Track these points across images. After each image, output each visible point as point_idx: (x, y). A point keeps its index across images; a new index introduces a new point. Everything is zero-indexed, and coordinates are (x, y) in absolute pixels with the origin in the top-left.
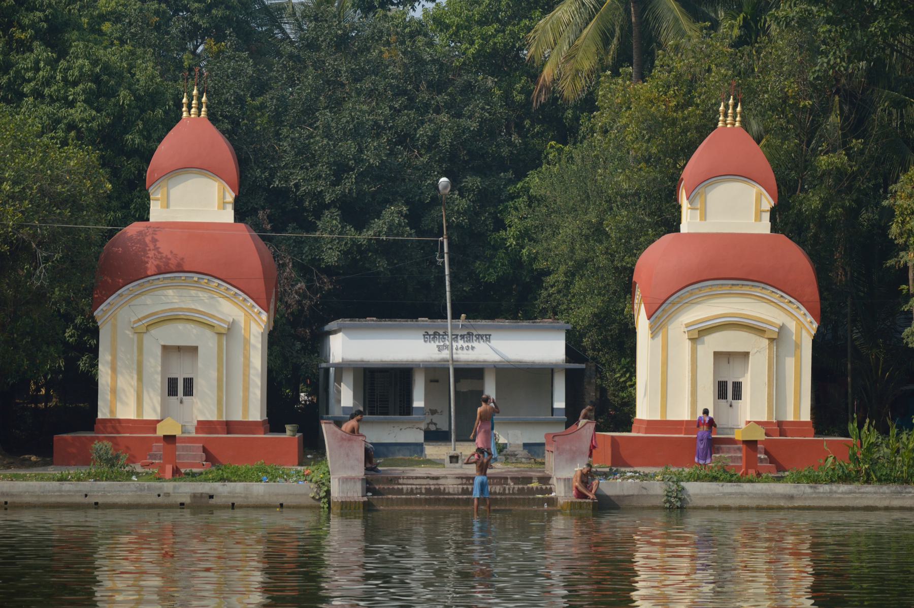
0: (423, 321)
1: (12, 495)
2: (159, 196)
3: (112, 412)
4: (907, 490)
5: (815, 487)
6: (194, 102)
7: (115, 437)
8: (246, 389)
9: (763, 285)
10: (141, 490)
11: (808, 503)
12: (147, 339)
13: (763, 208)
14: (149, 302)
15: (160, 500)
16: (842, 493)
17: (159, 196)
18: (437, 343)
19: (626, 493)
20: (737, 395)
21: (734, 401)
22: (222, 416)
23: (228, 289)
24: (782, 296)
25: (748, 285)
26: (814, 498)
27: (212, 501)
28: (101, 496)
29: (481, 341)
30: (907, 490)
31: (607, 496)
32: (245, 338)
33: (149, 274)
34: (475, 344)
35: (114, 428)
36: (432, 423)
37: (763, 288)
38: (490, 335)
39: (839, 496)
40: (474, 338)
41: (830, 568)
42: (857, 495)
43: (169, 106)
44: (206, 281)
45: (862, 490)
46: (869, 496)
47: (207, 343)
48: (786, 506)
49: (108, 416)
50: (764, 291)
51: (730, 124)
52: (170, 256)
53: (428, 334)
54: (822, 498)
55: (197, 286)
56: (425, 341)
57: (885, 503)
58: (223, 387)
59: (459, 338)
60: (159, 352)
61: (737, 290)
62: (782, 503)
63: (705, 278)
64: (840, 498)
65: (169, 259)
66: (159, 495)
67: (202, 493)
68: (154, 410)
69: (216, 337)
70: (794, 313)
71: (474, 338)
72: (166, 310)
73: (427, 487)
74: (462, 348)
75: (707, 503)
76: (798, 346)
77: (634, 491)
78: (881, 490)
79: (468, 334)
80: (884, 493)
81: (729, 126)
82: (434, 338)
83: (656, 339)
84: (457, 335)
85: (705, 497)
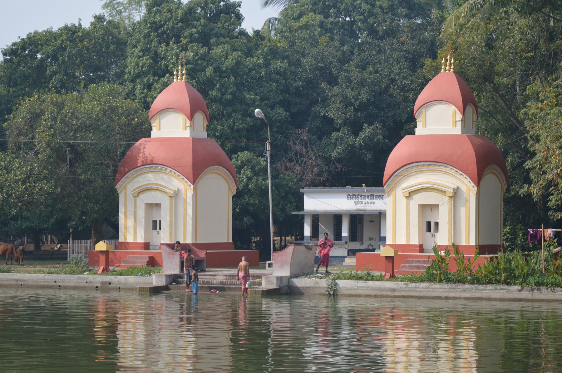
0: (349, 188)
1: (38, 281)
2: (155, 124)
3: (125, 238)
4: (458, 287)
5: (407, 284)
6: (179, 73)
7: (115, 252)
8: (185, 226)
9: (445, 165)
10: (79, 279)
11: (403, 294)
12: (138, 199)
13: (457, 119)
14: (141, 180)
15: (87, 285)
16: (422, 288)
17: (155, 124)
18: (355, 200)
19: (307, 286)
20: (436, 230)
21: (435, 233)
22: (172, 241)
23: (175, 173)
24: (456, 171)
25: (432, 165)
26: (406, 291)
27: (110, 286)
28: (62, 282)
29: (378, 199)
30: (458, 287)
31: (298, 287)
32: (184, 199)
33: (139, 165)
34: (375, 201)
35: (125, 246)
36: (370, 245)
37: (440, 165)
38: (383, 196)
39: (420, 290)
40: (375, 197)
41: (219, 332)
42: (430, 290)
43: (262, 75)
44: (160, 168)
45: (433, 287)
46: (437, 290)
47: (166, 203)
48: (391, 295)
49: (123, 241)
50: (446, 168)
51: (448, 70)
52: (148, 156)
53: (349, 195)
54: (410, 291)
55: (161, 171)
56: (348, 199)
57: (446, 295)
58: (174, 225)
59: (366, 197)
60: (143, 207)
61: (431, 168)
62: (389, 293)
63: (418, 161)
64: (420, 291)
65: (148, 157)
66: (87, 282)
67: (106, 282)
68: (142, 237)
69: (169, 198)
70: (464, 181)
71: (375, 197)
72: (150, 184)
73: (204, 280)
74: (368, 203)
75: (349, 292)
76: (468, 201)
77: (311, 285)
78: (444, 287)
79: (371, 195)
80: (445, 289)
81: (447, 71)
82: (352, 198)
83: (390, 197)
84: (365, 196)
85: (348, 289)
